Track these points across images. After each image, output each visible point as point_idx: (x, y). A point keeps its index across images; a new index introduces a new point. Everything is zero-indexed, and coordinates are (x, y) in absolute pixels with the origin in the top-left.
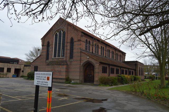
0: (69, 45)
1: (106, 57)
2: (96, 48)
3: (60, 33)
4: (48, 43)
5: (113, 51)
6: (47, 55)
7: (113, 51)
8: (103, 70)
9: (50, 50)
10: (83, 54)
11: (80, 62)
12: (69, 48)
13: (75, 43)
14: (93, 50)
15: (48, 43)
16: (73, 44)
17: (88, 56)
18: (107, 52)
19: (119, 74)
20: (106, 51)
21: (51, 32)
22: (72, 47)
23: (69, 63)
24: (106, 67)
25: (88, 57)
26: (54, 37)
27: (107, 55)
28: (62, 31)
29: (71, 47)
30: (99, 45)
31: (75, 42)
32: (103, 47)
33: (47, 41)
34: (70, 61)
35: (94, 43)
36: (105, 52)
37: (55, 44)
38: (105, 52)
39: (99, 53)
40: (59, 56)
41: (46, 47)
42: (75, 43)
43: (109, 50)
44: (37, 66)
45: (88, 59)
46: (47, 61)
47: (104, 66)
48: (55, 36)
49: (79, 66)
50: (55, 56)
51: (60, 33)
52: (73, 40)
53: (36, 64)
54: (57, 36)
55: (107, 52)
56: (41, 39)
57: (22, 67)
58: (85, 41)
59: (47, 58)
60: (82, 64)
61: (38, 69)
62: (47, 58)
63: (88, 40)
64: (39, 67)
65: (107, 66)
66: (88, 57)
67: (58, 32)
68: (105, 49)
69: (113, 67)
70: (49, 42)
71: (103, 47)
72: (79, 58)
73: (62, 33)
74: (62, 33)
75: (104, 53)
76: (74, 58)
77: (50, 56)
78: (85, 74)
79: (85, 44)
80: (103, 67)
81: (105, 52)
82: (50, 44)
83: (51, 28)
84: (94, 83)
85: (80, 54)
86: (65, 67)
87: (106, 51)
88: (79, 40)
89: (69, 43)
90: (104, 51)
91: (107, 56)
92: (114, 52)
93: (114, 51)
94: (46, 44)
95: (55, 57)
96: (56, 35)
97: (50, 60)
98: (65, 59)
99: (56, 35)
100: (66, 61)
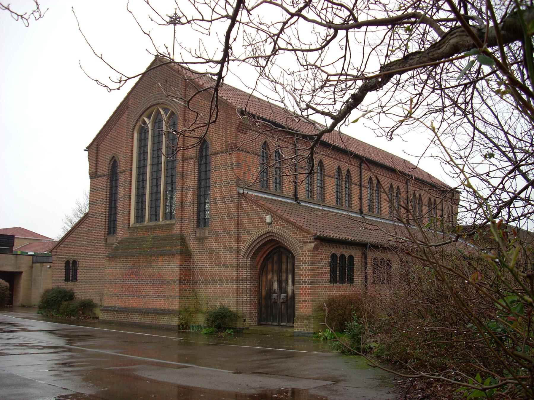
0: (191, 168)
1: (361, 212)
2: (371, 194)
3: (157, 121)
4: (114, 163)
5: (395, 184)
6: (110, 214)
7: (395, 184)
8: (333, 271)
9: (121, 192)
10: (247, 206)
11: (238, 242)
12: (191, 180)
13: (216, 161)
14: (361, 202)
15: (114, 163)
16: (207, 164)
17: (270, 211)
18: (365, 191)
19: (351, 281)
20: (360, 186)
21: (124, 118)
22: (206, 179)
23: (192, 245)
24: (351, 258)
25: (268, 219)
26: (133, 138)
27: (365, 201)
28: (166, 110)
29: (199, 180)
30: (327, 162)
31: (215, 154)
32: (348, 171)
33: (109, 156)
34: (198, 235)
35: (366, 175)
36: (355, 190)
37: (139, 168)
38: (355, 190)
39: (327, 197)
40: (155, 215)
41: (104, 182)
42: (214, 158)
43: (417, 196)
44: (75, 262)
45: (270, 224)
46: (112, 240)
47: (339, 251)
48: (140, 133)
49: (234, 254)
50: (140, 217)
51: (157, 121)
52: (207, 148)
53: (71, 254)
54: (146, 132)
55: (365, 191)
56: (88, 149)
57: (24, 265)
58: (260, 150)
59: (111, 229)
60: (244, 246)
61: (79, 272)
62: (111, 229)
63: (345, 166)
64: (81, 264)
65: (356, 253)
66: (268, 219)
67: (149, 117)
68: (355, 178)
69: (347, 252)
70: (115, 161)
71: (348, 171)
72: (235, 222)
73: (165, 118)
74: (165, 118)
75: (349, 195)
76: (212, 223)
77: (120, 217)
78: (260, 293)
79: (257, 161)
80: (334, 256)
81: (358, 191)
82: (121, 167)
83: (122, 104)
84: (295, 325)
85: (234, 205)
86: (176, 261)
87: (360, 186)
88: (233, 148)
89: (192, 162)
90: (349, 189)
91: (365, 209)
92: (402, 189)
93: (434, 194)
94: (104, 168)
95: (156, 220)
96: (143, 131)
97: (121, 233)
98: (176, 230)
99: (143, 131)
100: (182, 239)
